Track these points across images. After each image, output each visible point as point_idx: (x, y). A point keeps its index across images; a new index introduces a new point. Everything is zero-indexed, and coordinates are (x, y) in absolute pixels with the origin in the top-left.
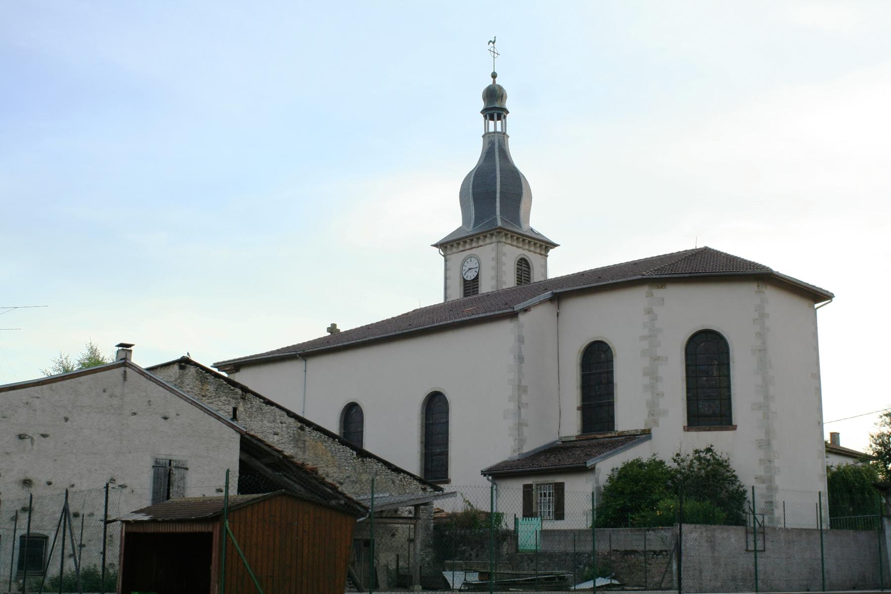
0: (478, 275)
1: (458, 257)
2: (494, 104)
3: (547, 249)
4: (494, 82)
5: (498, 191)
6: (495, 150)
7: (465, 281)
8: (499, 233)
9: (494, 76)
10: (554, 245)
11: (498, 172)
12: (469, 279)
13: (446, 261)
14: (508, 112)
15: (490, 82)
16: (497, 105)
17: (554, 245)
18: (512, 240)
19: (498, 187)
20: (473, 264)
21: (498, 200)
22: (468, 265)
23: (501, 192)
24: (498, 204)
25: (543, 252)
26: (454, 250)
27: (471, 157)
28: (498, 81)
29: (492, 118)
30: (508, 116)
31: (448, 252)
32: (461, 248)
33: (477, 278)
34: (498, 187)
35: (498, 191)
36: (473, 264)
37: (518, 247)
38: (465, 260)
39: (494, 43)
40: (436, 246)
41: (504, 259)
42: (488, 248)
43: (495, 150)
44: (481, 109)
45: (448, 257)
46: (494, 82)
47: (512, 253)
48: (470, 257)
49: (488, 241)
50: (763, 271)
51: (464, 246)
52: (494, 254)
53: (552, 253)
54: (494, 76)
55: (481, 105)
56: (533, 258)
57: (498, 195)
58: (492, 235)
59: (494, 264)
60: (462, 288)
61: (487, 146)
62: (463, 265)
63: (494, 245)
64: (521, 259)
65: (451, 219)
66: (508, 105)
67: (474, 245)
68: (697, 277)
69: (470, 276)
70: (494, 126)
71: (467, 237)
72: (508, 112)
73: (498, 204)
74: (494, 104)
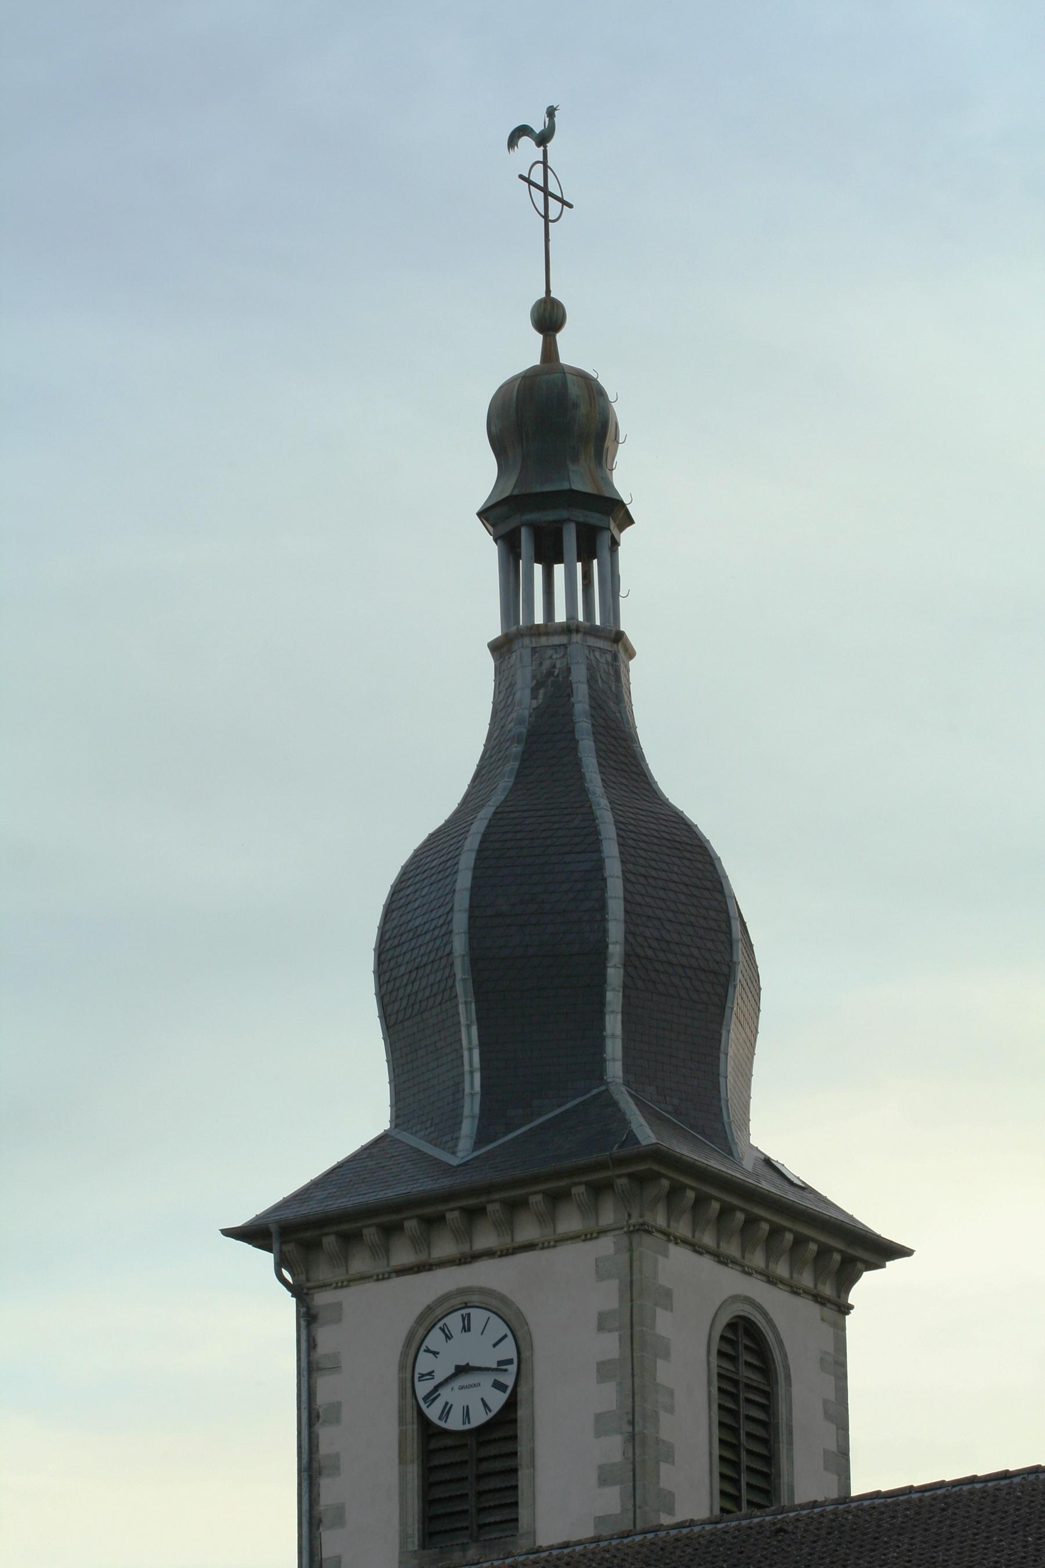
0: (511, 1404)
1: (381, 1308)
2: (553, 470)
3: (847, 1278)
4: (550, 351)
5: (616, 950)
6: (563, 716)
7: (428, 1430)
8: (641, 1180)
9: (549, 318)
10: (883, 1251)
11: (611, 849)
12: (455, 1423)
13: (308, 1319)
14: (629, 521)
15: (525, 352)
16: (580, 484)
17: (883, 1251)
18: (720, 1234)
19: (616, 931)
20: (481, 1343)
21: (614, 999)
22: (443, 1355)
23: (630, 958)
24: (614, 1024)
25: (827, 1290)
26: (360, 1263)
27: (428, 749)
28: (572, 351)
29: (549, 554)
30: (627, 538)
31: (324, 1273)
32: (403, 1255)
33: (505, 1426)
34: (616, 931)
35: (616, 950)
36: (481, 1343)
37: (722, 1259)
38: (429, 1319)
39: (543, 139)
40: (251, 1234)
41: (664, 1324)
42: (575, 1262)
43: (563, 716)
44: (479, 503)
45: (321, 1299)
46: (550, 351)
47: (698, 1286)
48: (462, 1302)
49: (570, 1222)
50: (834, 1214)
51: (423, 1242)
52: (607, 1296)
53: (869, 1289)
54: (549, 318)
55: (480, 474)
56: (787, 1316)
57: (614, 975)
58: (598, 1190)
59: (610, 1346)
60: (414, 1471)
61: (525, 701)
62: (414, 1345)
63: (606, 1245)
64: (732, 1326)
65: (331, 1096)
66: (628, 475)
67: (486, 1239)
68: (311, 1491)
69: (468, 1406)
70: (557, 594)
71: (448, 1197)
72: (629, 521)
73: (614, 1024)
74: (553, 470)
